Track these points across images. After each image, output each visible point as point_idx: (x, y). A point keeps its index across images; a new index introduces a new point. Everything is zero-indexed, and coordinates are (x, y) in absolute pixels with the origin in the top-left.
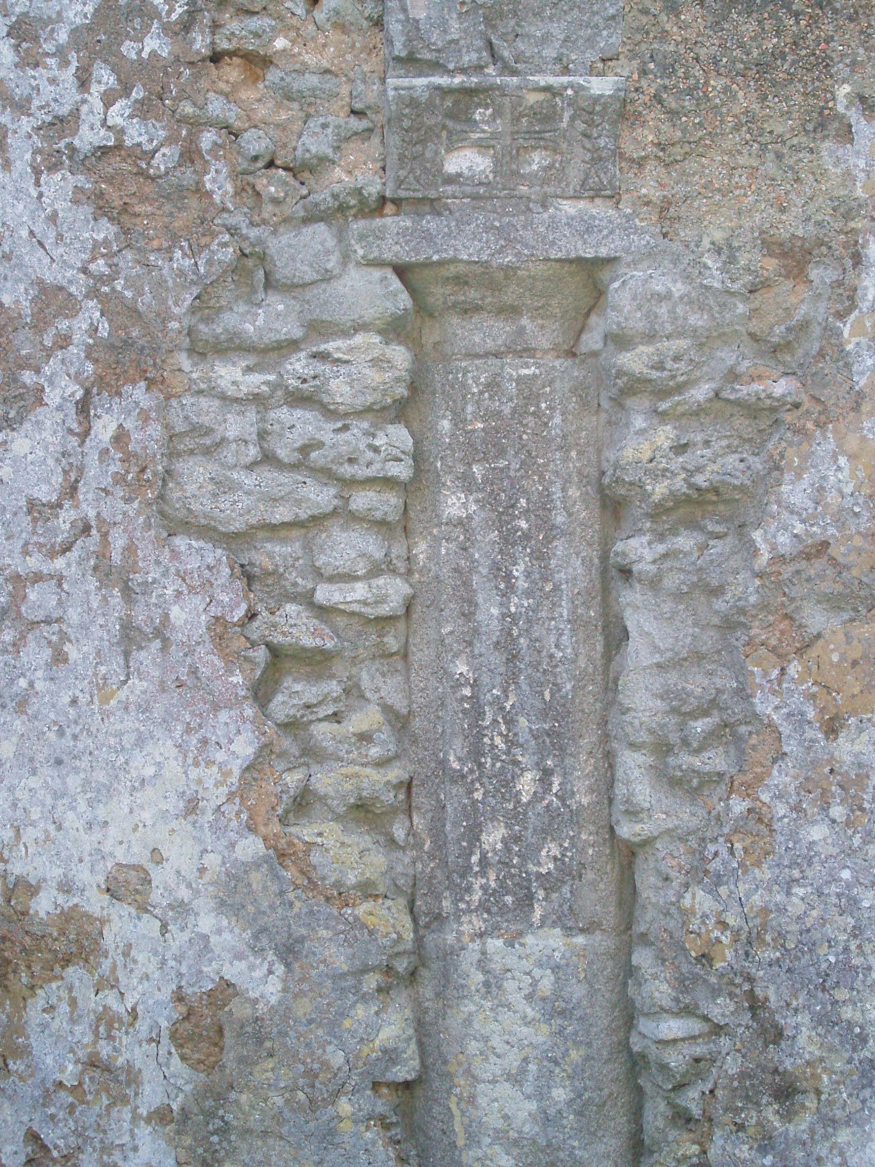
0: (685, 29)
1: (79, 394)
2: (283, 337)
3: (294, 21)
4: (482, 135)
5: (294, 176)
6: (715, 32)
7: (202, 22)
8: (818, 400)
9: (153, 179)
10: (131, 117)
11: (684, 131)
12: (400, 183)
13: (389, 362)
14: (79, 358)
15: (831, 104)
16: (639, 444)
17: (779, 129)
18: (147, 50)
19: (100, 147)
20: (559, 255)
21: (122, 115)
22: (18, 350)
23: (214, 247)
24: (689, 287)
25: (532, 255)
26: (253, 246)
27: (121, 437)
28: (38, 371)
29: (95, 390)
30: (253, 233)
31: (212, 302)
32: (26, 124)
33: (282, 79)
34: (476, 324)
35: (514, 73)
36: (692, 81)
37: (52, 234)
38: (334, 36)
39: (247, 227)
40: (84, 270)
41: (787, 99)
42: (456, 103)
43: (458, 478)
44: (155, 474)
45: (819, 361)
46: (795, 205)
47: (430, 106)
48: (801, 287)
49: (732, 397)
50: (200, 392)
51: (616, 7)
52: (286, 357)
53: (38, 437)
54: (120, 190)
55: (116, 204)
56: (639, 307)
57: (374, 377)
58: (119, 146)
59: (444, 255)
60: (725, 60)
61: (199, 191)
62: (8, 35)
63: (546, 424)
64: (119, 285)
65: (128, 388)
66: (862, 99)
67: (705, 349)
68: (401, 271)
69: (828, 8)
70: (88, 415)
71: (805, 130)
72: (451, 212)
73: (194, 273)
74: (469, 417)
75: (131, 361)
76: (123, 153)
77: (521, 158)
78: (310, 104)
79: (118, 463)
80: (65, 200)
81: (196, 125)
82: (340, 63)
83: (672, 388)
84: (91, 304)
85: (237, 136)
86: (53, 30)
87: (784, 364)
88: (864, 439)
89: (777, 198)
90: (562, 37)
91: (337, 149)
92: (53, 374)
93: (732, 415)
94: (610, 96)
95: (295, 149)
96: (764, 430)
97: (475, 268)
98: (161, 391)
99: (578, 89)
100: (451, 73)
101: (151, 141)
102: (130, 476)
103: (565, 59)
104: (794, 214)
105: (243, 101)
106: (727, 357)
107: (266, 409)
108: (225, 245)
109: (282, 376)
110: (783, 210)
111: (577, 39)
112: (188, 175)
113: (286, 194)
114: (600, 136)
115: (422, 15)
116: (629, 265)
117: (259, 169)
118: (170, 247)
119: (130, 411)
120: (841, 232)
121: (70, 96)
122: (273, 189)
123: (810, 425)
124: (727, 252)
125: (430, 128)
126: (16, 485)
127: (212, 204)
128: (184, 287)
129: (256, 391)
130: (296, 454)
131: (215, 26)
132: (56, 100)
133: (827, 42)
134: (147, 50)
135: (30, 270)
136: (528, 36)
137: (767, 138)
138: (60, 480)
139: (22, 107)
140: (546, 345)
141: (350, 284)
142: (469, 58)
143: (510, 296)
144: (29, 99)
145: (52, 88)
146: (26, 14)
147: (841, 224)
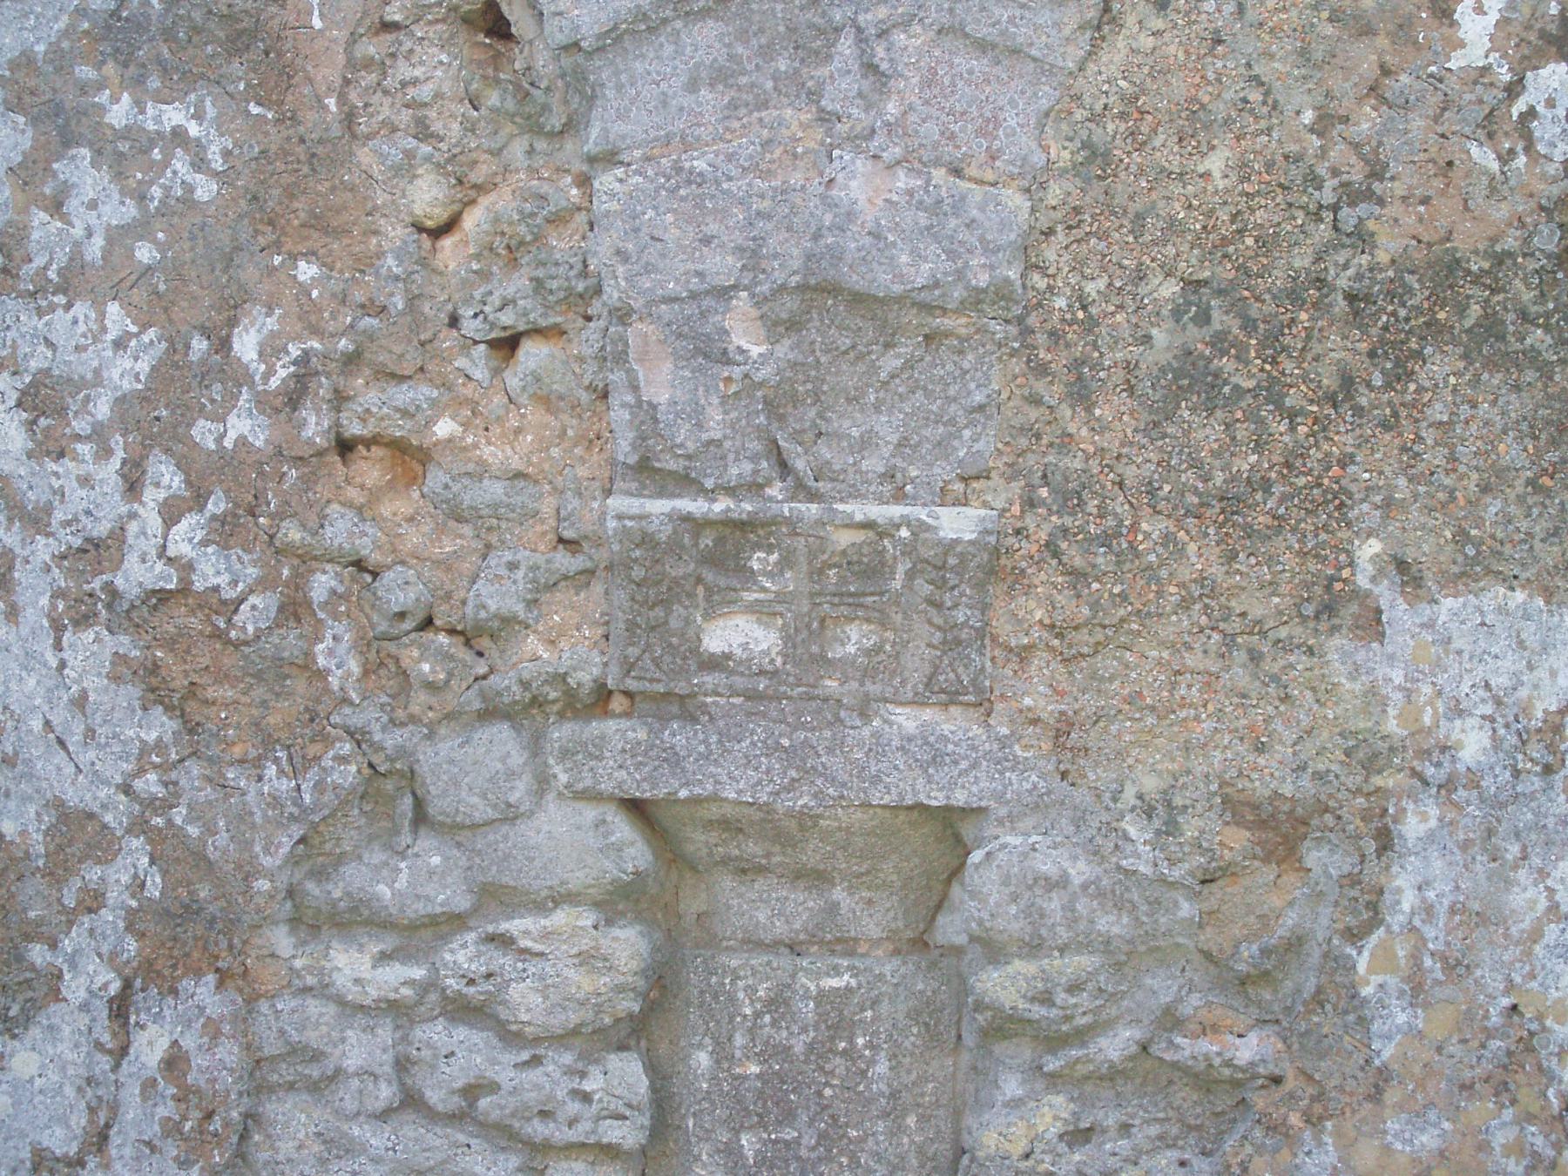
0: (1101, 433)
1: (115, 987)
2: (439, 910)
3: (468, 391)
4: (761, 596)
5: (468, 643)
6: (1152, 441)
7: (317, 394)
8: (1310, 1078)
9: (237, 645)
10: (205, 543)
11: (1095, 606)
12: (628, 667)
13: (606, 960)
14: (115, 928)
15: (1345, 573)
16: (1009, 1125)
17: (1257, 612)
18: (232, 435)
19: (154, 592)
20: (886, 800)
21: (190, 540)
22: (25, 910)
23: (327, 762)
24: (1099, 870)
25: (842, 797)
26: (393, 761)
27: (174, 1062)
28: (53, 945)
29: (138, 983)
30: (392, 740)
31: (328, 846)
32: (44, 550)
33: (446, 487)
34: (760, 893)
35: (813, 496)
36: (1110, 522)
37: (79, 728)
38: (533, 414)
39: (384, 729)
40: (127, 789)
41: (1271, 560)
42: (720, 541)
43: (719, 1151)
44: (227, 1124)
45: (1313, 1012)
46: (1281, 742)
47: (674, 547)
48: (1290, 879)
49: (1167, 1057)
50: (306, 990)
51: (986, 392)
52: (444, 938)
53: (51, 1052)
54: (185, 662)
55: (176, 684)
56: (1015, 898)
57: (582, 982)
58: (185, 590)
59: (697, 790)
60: (1167, 488)
61: (307, 665)
62: (19, 404)
63: (864, 1073)
64: (179, 815)
65: (187, 984)
66: (1402, 565)
67: (1126, 970)
68: (636, 808)
69: (1347, 406)
70: (126, 1023)
71: (1300, 615)
72: (711, 719)
73: (295, 804)
74: (738, 1054)
75: (196, 938)
76: (190, 601)
77: (829, 633)
78: (489, 529)
79: (171, 1103)
80: (100, 674)
81: (308, 560)
82: (542, 460)
83: (1067, 1035)
84: (136, 843)
85: (375, 575)
86: (87, 399)
87: (1259, 1004)
88: (1387, 1149)
89: (1251, 728)
90: (894, 438)
91: (532, 603)
92: (75, 952)
93: (1171, 1082)
94: (971, 542)
95: (464, 602)
96: (1223, 1113)
97: (746, 810)
98: (240, 991)
99: (919, 528)
100: (710, 495)
101: (235, 583)
102: (188, 1126)
103: (899, 475)
104: (1278, 757)
105: (385, 520)
106: (1161, 987)
107: (412, 1022)
108: (343, 760)
109: (437, 970)
110: (1260, 749)
111: (919, 444)
112: (290, 641)
113: (450, 675)
114: (956, 606)
115: (663, 398)
116: (1001, 822)
117: (408, 633)
118: (259, 758)
119: (190, 1021)
120: (1358, 792)
121: (113, 505)
122: (426, 667)
123: (1295, 1119)
124: (1163, 813)
125: (676, 581)
126: (16, 1125)
127: (327, 690)
128: (279, 825)
129: (392, 996)
130: (456, 1099)
131: (340, 399)
132: (88, 513)
133: (1343, 465)
134: (232, 435)
135: (44, 784)
136: (838, 436)
137: (1236, 625)
138: (83, 1122)
139: (37, 521)
140: (875, 932)
141: (546, 828)
142: (737, 471)
143: (812, 854)
144: (48, 510)
145: (83, 493)
146: (47, 372)
147: (1359, 778)
